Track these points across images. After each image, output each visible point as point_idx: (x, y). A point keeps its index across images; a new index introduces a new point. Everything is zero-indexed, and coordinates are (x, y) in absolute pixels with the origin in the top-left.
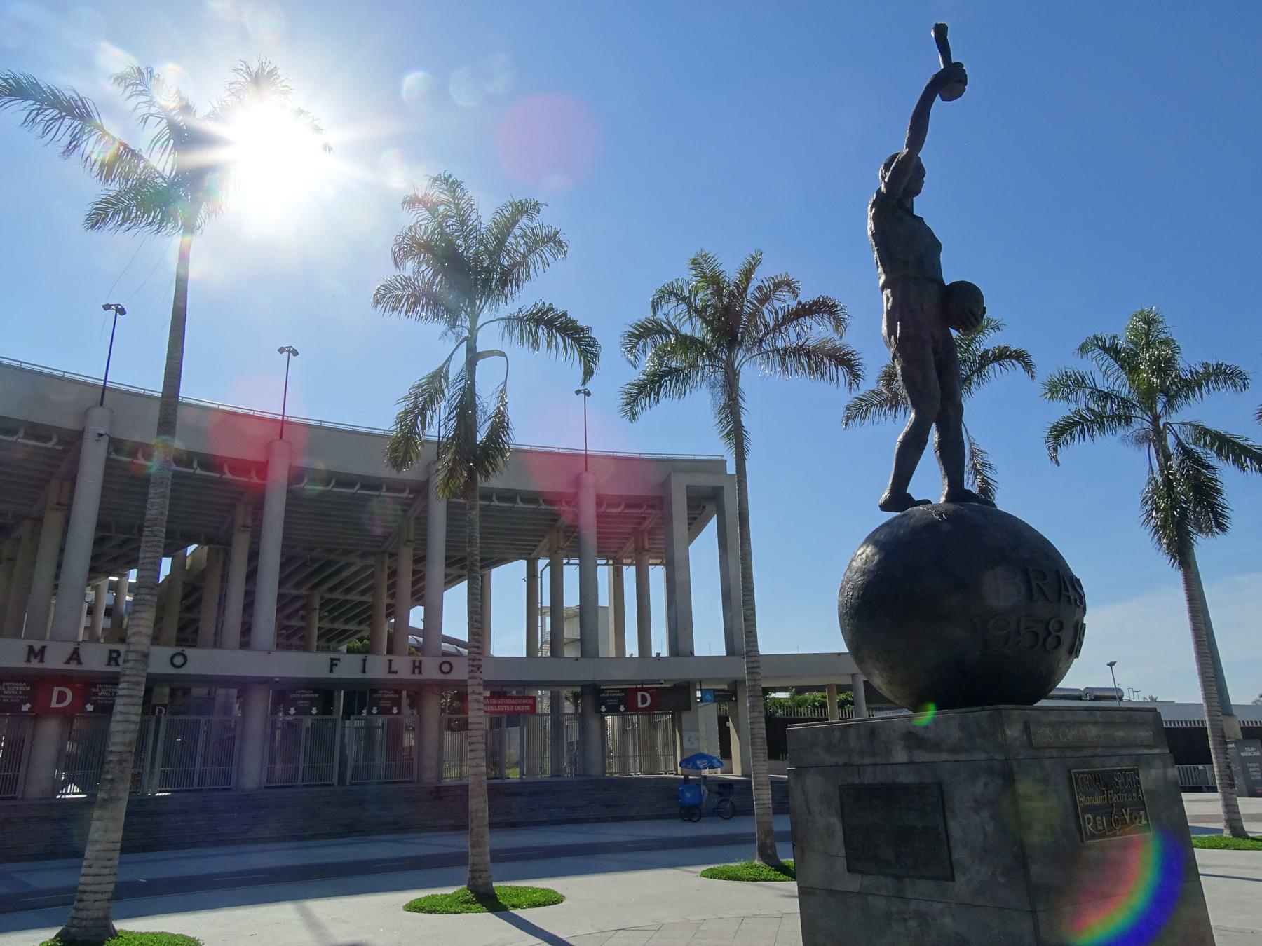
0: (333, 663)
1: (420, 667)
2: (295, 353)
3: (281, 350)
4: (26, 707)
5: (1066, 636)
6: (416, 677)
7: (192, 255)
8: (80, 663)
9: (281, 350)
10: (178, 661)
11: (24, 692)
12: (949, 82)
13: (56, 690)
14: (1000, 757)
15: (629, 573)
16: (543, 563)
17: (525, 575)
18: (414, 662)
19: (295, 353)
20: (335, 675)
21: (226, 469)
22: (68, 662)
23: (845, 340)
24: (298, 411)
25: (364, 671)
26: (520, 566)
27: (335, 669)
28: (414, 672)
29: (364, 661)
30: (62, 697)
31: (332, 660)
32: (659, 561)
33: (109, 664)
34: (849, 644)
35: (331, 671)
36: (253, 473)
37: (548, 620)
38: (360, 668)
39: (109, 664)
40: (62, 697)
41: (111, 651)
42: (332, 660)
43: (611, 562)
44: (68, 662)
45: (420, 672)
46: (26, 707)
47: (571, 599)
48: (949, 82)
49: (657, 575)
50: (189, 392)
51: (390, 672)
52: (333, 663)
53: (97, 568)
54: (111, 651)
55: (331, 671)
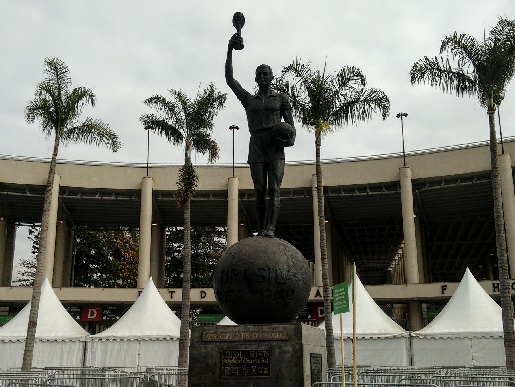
4: (309, 317)
7: (148, 97)
11: (308, 310)
13: (90, 310)
18: (494, 284)
20: (205, 300)
22: (316, 296)
23: (369, 86)
24: (412, 147)
25: (172, 298)
27: (445, 291)
28: (494, 291)
30: (92, 313)
31: (443, 286)
34: (465, 270)
35: (443, 293)
39: (202, 297)
40: (92, 313)
42: (443, 286)
44: (316, 296)
46: (309, 317)
55: (443, 293)
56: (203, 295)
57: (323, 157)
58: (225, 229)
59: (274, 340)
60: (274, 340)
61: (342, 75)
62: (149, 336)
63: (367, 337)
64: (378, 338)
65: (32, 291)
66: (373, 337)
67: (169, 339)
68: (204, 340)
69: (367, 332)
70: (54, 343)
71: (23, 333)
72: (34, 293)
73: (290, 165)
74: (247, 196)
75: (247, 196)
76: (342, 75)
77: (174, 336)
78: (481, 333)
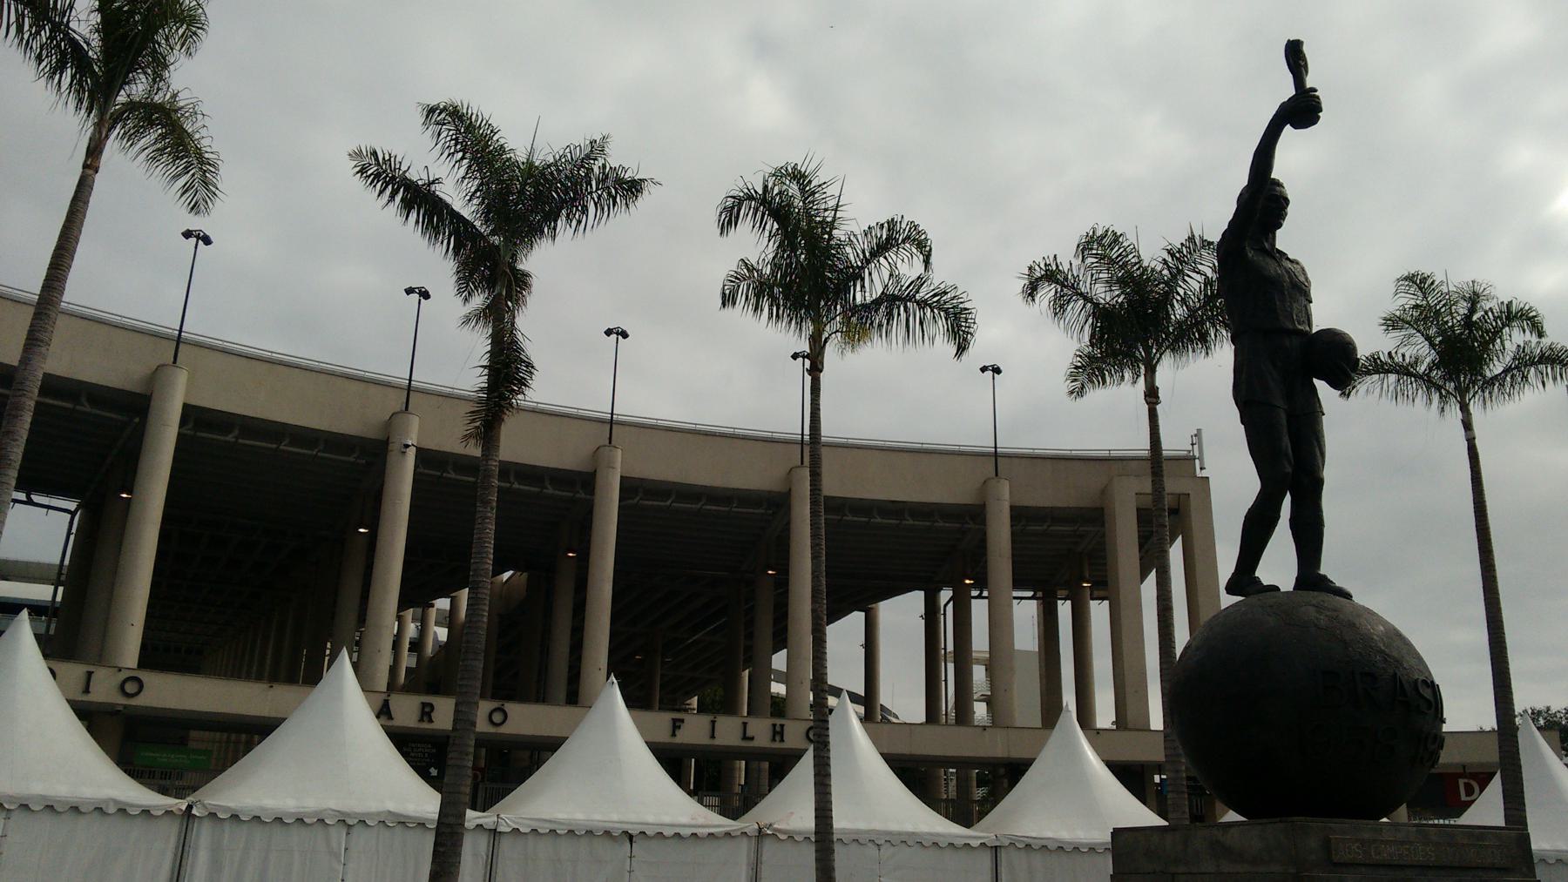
0: (676, 725)
1: (775, 733)
2: (625, 335)
3: (609, 332)
5: (1427, 693)
6: (777, 745)
8: (431, 721)
9: (609, 332)
10: (130, 688)
12: (1301, 110)
13: (1461, 782)
14: (1292, 871)
15: (1064, 609)
16: (945, 595)
17: (922, 611)
19: (625, 335)
20: (679, 739)
21: (83, 399)
25: (713, 737)
26: (916, 599)
28: (774, 740)
29: (713, 722)
31: (674, 721)
32: (1030, 594)
33: (421, 720)
35: (674, 735)
36: (83, 399)
37: (951, 667)
38: (81, 687)
39: (421, 720)
41: (424, 705)
42: (674, 721)
43: (1040, 594)
45: (782, 740)
47: (980, 640)
48: (1301, 110)
49: (1099, 612)
50: (828, 431)
51: (745, 738)
52: (676, 725)
53: (415, 595)
54: (424, 705)
55: (674, 735)
56: (426, 712)
57: (75, 293)
58: (28, 496)
59: (1484, 869)
60: (1484, 869)
61: (730, 222)
62: (44, 797)
63: (668, 832)
64: (711, 834)
65: (453, 707)
66: (699, 831)
67: (112, 810)
68: (1336, 859)
69: (667, 819)
70: (530, 837)
71: (805, 820)
72: (456, 711)
73: (72, 315)
74: (236, 432)
75: (236, 432)
76: (730, 222)
77: (129, 800)
78: (900, 834)
